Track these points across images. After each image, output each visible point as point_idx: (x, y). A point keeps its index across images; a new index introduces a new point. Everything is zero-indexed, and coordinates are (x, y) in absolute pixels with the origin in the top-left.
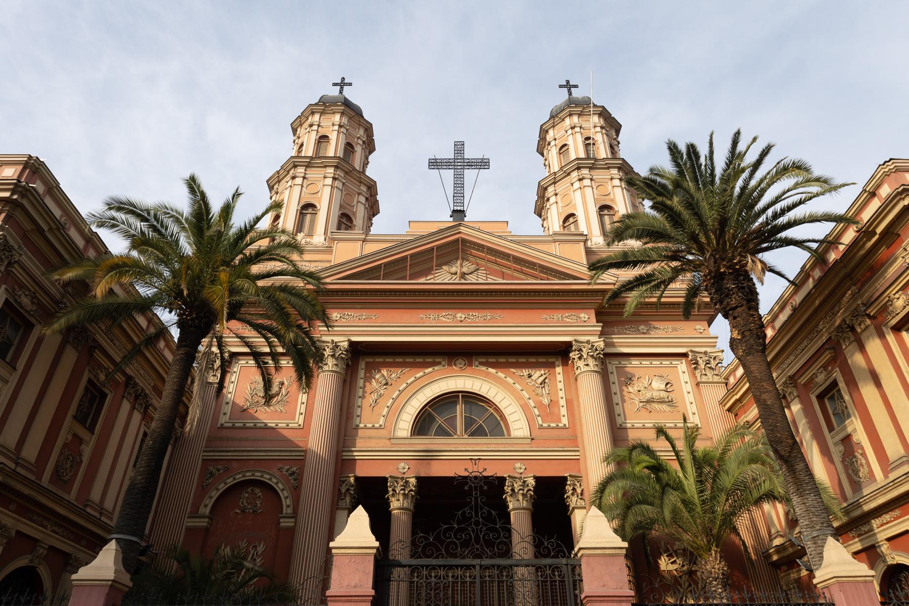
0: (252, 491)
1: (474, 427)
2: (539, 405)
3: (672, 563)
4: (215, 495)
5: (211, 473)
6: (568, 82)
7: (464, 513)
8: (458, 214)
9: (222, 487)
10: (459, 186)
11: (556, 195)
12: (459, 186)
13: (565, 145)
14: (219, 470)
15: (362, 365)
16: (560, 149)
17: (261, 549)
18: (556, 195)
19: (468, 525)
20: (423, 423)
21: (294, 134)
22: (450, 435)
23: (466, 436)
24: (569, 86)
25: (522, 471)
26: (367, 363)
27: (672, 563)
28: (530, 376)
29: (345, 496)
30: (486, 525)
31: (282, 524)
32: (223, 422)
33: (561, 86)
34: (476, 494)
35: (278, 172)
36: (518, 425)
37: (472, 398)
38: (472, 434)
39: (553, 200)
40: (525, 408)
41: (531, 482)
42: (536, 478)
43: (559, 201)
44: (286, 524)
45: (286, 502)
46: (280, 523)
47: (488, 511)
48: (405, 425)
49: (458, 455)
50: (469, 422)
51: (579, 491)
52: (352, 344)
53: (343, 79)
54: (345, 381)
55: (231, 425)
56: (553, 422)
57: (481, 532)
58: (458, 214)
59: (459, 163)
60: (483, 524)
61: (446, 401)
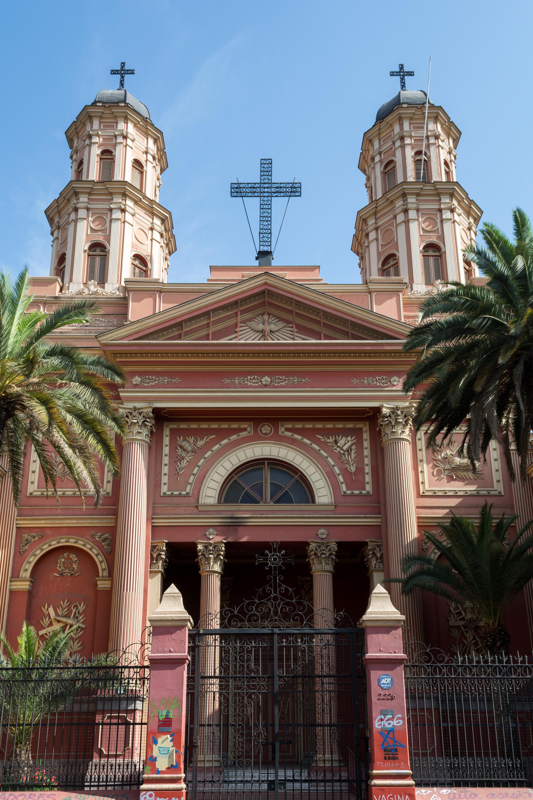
0: (68, 556)
1: (280, 494)
2: (345, 472)
3: (460, 620)
4: (33, 560)
5: (27, 540)
6: (402, 67)
7: (264, 590)
8: (264, 255)
9: (39, 553)
10: (266, 218)
11: (376, 229)
12: (266, 218)
13: (391, 162)
14: (34, 537)
15: (167, 432)
16: (385, 167)
17: (82, 608)
18: (376, 229)
19: (268, 601)
20: (234, 489)
21: (71, 147)
22: (255, 501)
23: (272, 504)
24: (402, 74)
25: (324, 536)
26: (172, 430)
27: (460, 620)
28: (336, 442)
29: (157, 560)
30: (283, 600)
31: (99, 586)
32: (32, 491)
33: (392, 74)
34: (275, 573)
35: (57, 201)
36: (323, 494)
37: (278, 465)
38: (277, 502)
39: (372, 236)
40: (330, 476)
41: (334, 547)
42: (337, 543)
43: (380, 237)
44: (103, 586)
45: (102, 566)
46: (97, 585)
47: (286, 589)
48: (210, 492)
49: (267, 521)
50: (275, 488)
51: (379, 555)
52: (156, 411)
53: (123, 64)
54: (150, 448)
55: (39, 493)
56: (357, 490)
57: (279, 605)
58: (264, 255)
59: (266, 189)
60: (281, 599)
61: (255, 465)
